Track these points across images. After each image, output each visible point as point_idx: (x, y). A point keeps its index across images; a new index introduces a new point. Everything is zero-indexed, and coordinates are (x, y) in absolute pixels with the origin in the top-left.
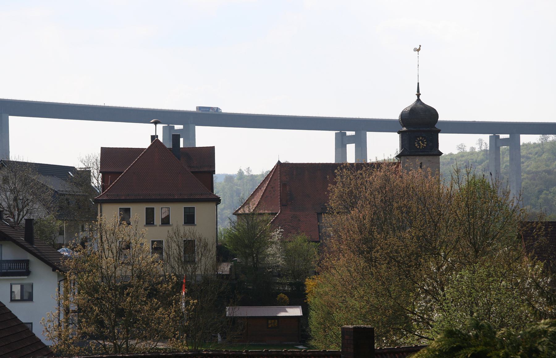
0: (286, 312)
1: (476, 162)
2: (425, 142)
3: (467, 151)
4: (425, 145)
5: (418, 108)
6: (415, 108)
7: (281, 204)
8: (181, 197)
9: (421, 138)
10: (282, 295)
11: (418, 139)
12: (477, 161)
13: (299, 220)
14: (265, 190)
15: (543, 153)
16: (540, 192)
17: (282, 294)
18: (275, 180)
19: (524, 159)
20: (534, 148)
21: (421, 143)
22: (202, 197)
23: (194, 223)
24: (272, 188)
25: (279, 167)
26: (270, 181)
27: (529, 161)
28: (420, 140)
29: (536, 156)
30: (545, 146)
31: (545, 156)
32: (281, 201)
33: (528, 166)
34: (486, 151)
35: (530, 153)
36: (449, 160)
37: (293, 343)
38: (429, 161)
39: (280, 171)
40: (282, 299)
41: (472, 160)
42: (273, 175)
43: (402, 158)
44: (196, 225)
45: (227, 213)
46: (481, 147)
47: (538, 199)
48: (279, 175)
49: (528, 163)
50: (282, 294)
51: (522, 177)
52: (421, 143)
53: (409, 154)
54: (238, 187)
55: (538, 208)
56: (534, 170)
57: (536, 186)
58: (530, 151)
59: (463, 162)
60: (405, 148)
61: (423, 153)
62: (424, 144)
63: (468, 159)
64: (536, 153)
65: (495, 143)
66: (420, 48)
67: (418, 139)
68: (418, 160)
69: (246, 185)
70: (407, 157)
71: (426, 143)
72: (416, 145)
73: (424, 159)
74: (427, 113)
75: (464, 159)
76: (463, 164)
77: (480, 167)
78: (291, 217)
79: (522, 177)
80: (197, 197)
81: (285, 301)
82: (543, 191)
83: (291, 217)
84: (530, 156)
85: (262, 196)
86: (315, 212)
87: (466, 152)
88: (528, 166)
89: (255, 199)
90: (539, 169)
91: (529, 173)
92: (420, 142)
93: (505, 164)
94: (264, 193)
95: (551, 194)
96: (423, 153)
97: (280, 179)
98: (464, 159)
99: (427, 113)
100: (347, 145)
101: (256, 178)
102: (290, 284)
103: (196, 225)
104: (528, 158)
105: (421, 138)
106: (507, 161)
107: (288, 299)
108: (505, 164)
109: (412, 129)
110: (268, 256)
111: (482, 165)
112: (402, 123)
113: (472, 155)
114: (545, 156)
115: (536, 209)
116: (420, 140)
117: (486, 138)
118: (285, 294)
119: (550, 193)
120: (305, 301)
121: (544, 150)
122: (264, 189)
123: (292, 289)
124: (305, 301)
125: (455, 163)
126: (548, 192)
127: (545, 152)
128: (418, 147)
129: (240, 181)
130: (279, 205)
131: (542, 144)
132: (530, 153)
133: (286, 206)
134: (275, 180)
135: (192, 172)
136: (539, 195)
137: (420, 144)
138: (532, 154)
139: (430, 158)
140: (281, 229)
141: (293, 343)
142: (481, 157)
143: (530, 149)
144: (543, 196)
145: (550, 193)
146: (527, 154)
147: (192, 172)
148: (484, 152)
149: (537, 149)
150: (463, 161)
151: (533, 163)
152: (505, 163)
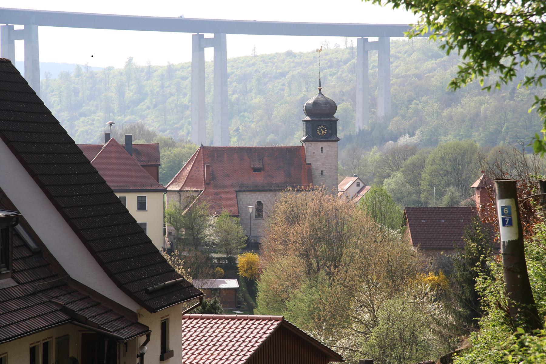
0: (225, 283)
1: (341, 61)
2: (326, 130)
3: (331, 48)
4: (325, 133)
5: (320, 101)
6: (317, 101)
7: (204, 183)
8: (135, 188)
9: (322, 127)
10: (219, 269)
11: (320, 127)
12: (342, 60)
13: (221, 197)
14: (191, 170)
15: (413, 52)
16: (410, 101)
17: (218, 267)
18: (199, 161)
19: (393, 58)
20: (403, 45)
21: (322, 131)
22: (152, 188)
23: (145, 209)
24: (197, 168)
25: (202, 150)
26: (194, 162)
27: (398, 61)
28: (321, 128)
29: (405, 55)
30: (415, 44)
31: (414, 56)
32: (205, 180)
33: (397, 67)
34: (352, 48)
35: (399, 52)
36: (312, 58)
37: (231, 309)
38: (329, 146)
39: (203, 153)
40: (219, 271)
41: (337, 58)
42: (197, 157)
43: (307, 143)
44: (147, 211)
45: (64, 115)
46: (346, 44)
47: (408, 109)
48: (202, 157)
49: (397, 63)
50: (218, 267)
51: (391, 82)
52: (322, 131)
53: (312, 140)
54: (76, 86)
55: (407, 119)
56: (404, 73)
57: (406, 93)
58: (398, 49)
59: (326, 61)
60: (309, 135)
61: (324, 139)
62: (324, 131)
63: (333, 57)
64: (406, 52)
65: (364, 46)
66: (321, 49)
67: (320, 127)
68: (320, 145)
69: (85, 84)
70: (311, 142)
71: (326, 131)
72: (318, 132)
73: (324, 144)
74: (327, 105)
75: (328, 57)
76: (327, 64)
77: (345, 67)
78: (214, 195)
79: (391, 82)
80: (148, 188)
81: (221, 273)
82: (413, 101)
83: (214, 195)
84: (400, 55)
85: (188, 175)
86: (234, 190)
87: (330, 50)
88: (397, 67)
89: (182, 176)
90: (409, 73)
91: (397, 76)
92: (322, 130)
93: (372, 65)
94: (189, 173)
95: (422, 103)
96: (324, 139)
97: (204, 161)
98: (328, 57)
99: (327, 105)
100: (205, 48)
101: (96, 76)
102: (224, 259)
103: (147, 211)
104: (397, 58)
105: (322, 127)
106: (375, 61)
107: (223, 272)
108: (372, 65)
109: (315, 119)
110: (205, 236)
111: (347, 65)
112: (305, 111)
113: (337, 53)
114: (414, 56)
115: (405, 120)
116: (321, 128)
117: (353, 41)
118: (220, 266)
119: (420, 102)
120: (238, 274)
121: (414, 49)
122: (189, 168)
123: (225, 262)
124: (238, 274)
125: (318, 62)
126: (418, 102)
127: (415, 51)
128: (320, 134)
129: (77, 78)
130: (203, 184)
131: (412, 43)
132: (399, 52)
133: (209, 184)
134: (199, 161)
135: (142, 165)
136: (409, 105)
137: (321, 131)
138: (400, 53)
139: (330, 143)
140: (216, 214)
141: (231, 309)
142: (346, 56)
143: (399, 47)
144: (412, 106)
145: (420, 102)
146: (396, 53)
147: (142, 165)
148: (349, 50)
149: (406, 47)
150: (327, 60)
151: (402, 63)
152: (372, 63)
